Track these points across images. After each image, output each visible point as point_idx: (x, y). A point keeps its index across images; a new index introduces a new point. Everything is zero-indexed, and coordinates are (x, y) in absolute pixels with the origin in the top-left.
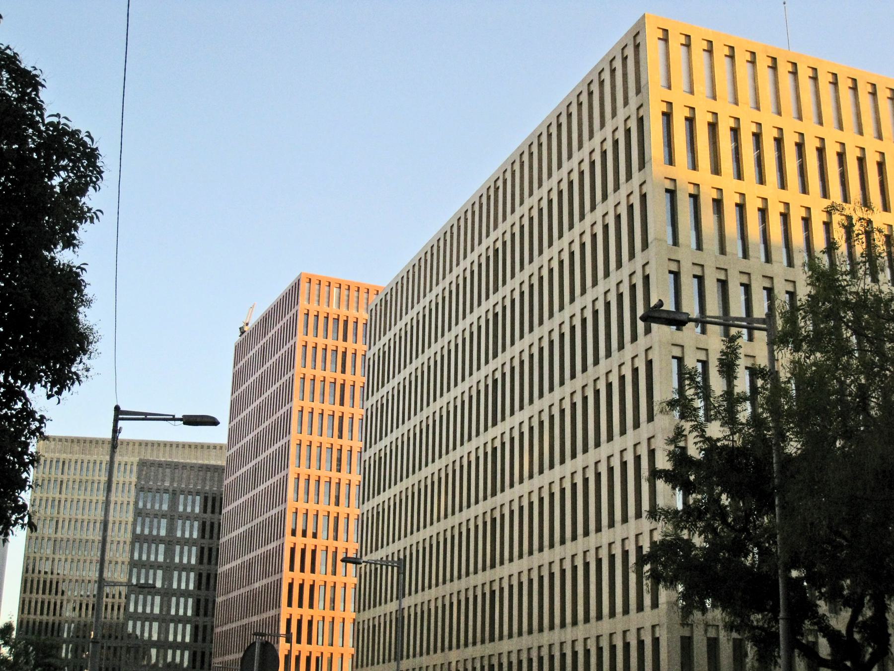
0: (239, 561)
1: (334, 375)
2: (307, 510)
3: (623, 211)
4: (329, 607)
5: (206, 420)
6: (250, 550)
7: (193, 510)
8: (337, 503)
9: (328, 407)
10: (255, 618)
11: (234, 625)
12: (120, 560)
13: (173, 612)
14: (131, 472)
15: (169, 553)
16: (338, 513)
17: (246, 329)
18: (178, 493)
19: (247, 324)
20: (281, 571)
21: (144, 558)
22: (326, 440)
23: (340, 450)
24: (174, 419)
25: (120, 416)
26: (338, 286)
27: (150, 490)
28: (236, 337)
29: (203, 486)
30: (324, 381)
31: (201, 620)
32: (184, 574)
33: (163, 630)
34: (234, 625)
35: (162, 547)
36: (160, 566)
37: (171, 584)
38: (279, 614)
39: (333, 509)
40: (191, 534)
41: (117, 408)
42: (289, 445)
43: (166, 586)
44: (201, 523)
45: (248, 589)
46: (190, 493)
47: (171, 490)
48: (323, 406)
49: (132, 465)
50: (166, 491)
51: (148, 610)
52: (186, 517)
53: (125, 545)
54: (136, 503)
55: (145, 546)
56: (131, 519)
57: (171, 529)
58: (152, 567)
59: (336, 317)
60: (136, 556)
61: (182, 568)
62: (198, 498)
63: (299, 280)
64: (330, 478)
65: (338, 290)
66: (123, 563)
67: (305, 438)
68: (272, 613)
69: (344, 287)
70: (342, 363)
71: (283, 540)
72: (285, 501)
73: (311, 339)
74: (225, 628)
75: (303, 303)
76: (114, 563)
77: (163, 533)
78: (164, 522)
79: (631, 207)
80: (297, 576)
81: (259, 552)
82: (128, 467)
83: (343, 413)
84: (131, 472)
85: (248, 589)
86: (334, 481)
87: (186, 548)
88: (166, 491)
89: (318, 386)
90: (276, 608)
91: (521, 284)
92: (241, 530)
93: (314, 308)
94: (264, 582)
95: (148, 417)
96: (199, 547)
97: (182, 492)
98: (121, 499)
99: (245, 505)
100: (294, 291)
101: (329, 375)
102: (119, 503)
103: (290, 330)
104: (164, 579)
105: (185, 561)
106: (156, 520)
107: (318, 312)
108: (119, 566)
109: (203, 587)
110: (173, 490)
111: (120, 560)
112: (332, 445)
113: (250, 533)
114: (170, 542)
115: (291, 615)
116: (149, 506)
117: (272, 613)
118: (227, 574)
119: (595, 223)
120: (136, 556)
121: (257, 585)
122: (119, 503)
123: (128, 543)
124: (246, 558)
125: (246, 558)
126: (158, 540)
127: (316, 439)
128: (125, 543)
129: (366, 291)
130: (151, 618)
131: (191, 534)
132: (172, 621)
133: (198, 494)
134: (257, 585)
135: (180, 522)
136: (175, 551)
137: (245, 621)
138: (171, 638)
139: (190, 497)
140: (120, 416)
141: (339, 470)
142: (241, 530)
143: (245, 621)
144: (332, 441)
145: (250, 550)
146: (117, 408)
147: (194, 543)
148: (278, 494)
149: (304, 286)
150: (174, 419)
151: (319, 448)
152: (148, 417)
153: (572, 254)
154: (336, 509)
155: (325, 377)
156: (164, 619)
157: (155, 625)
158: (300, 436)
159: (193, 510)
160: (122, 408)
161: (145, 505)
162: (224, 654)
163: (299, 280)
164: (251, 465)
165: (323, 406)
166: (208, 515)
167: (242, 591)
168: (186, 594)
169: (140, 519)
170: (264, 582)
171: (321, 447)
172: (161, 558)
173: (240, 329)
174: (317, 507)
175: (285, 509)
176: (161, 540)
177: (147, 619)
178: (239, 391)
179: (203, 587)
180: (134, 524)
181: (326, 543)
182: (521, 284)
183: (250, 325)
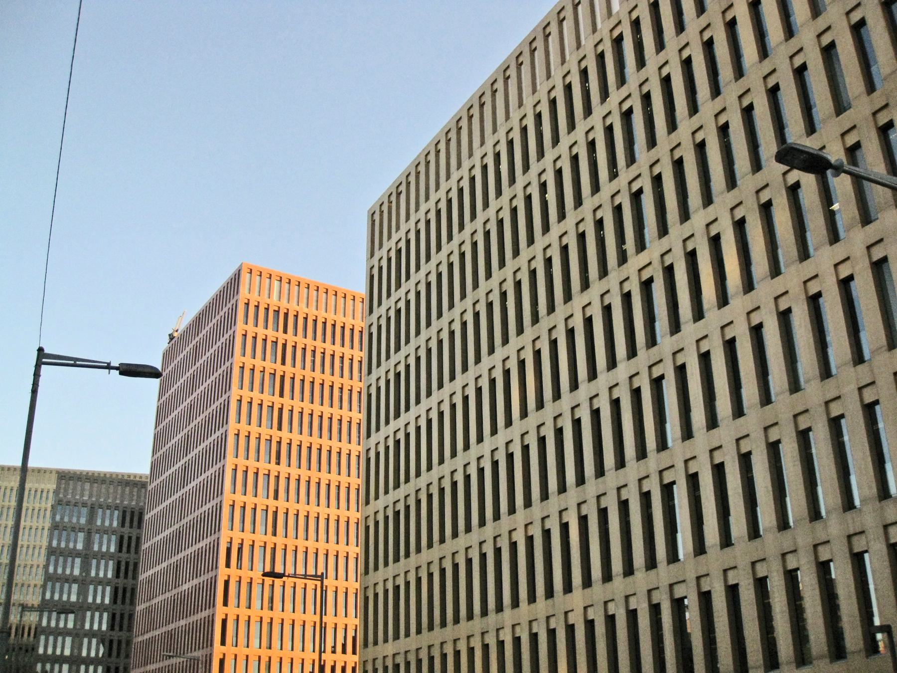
0: (165, 565)
1: (273, 366)
2: (245, 503)
3: (469, 318)
4: (267, 607)
5: (146, 370)
6: (178, 550)
7: (111, 524)
8: (276, 497)
9: (267, 399)
10: (183, 622)
11: (157, 632)
12: (32, 583)
13: (87, 626)
14: (47, 498)
15: (86, 567)
16: (277, 508)
17: (176, 334)
18: (96, 507)
19: (177, 331)
20: (216, 568)
21: (60, 571)
22: (265, 431)
23: (279, 443)
24: (109, 367)
25: (44, 360)
26: (279, 279)
27: (65, 528)
28: (164, 344)
29: (122, 501)
30: (264, 371)
31: (116, 635)
32: (100, 588)
33: (76, 645)
34: (157, 632)
35: (75, 587)
36: (75, 580)
37: (86, 598)
38: (213, 615)
39: (272, 503)
40: (108, 547)
41: (41, 350)
42: (226, 436)
43: (80, 601)
44: (119, 537)
45: (174, 592)
46: (109, 507)
47: (89, 504)
48: (262, 397)
49: (48, 492)
50: (84, 505)
51: (58, 652)
52: (103, 531)
53: (35, 588)
54: (46, 567)
55: (61, 559)
56: (40, 582)
57: (88, 542)
58: (67, 581)
59: (277, 309)
60: (55, 543)
61: (98, 582)
62: (116, 512)
63: (239, 271)
64: (269, 471)
65: (279, 282)
66: (35, 586)
67: (244, 427)
68: (205, 614)
69: (285, 281)
70: (282, 357)
71: (219, 534)
72: (222, 494)
73: (251, 329)
74: (147, 636)
75: (244, 293)
76: (26, 586)
77: (80, 546)
78: (81, 536)
79: (464, 324)
80: (233, 571)
81: (191, 550)
82: (45, 494)
83: (282, 405)
84: (47, 498)
85: (174, 592)
86: (273, 474)
87: (103, 562)
88: (84, 505)
89: (258, 375)
90: (209, 608)
91: (387, 372)
92: (167, 532)
93: (254, 299)
94: (195, 582)
95: (77, 363)
96: (116, 561)
97: (101, 507)
98: (33, 543)
99: (172, 506)
100: (235, 280)
101: (269, 365)
102: (34, 528)
103: (231, 319)
104: (78, 594)
105: (101, 575)
106: (66, 585)
107: (259, 302)
108: (31, 589)
109: (119, 601)
110: (92, 504)
111: (32, 583)
112: (271, 436)
113: (179, 534)
114: (87, 557)
115: (226, 615)
116: (66, 519)
117: (205, 614)
118: (150, 581)
119: (441, 330)
120: (55, 543)
121: (185, 587)
122: (34, 528)
123: (41, 566)
124: (174, 559)
125: (174, 559)
126: (75, 554)
127: (254, 429)
128: (38, 566)
129: (306, 286)
130: (65, 633)
131: (108, 547)
132: (86, 635)
133: (117, 508)
134: (185, 587)
135: (97, 536)
136: (91, 565)
137: (171, 626)
138: (84, 654)
139: (105, 536)
140: (44, 360)
141: (278, 463)
142: (167, 532)
143: (171, 626)
144: (271, 432)
145: (178, 550)
146: (41, 350)
147: (111, 557)
148: (215, 487)
149: (245, 277)
150: (109, 367)
151: (258, 440)
152: (77, 363)
153: (429, 351)
154: (275, 503)
155: (264, 368)
156: (78, 635)
157: (69, 640)
158: (238, 426)
159: (111, 524)
160: (47, 351)
161: (62, 519)
162: (146, 664)
163: (239, 271)
164: (180, 464)
165: (262, 397)
166: (126, 530)
167: (168, 595)
168: (101, 608)
169: (56, 532)
170: (195, 582)
171: (259, 438)
172: (77, 572)
173: (170, 335)
174: (255, 500)
175: (221, 502)
176: (78, 554)
177: (60, 634)
178: (167, 395)
179: (119, 601)
180: (44, 587)
181: (264, 538)
182: (387, 372)
183: (179, 332)
